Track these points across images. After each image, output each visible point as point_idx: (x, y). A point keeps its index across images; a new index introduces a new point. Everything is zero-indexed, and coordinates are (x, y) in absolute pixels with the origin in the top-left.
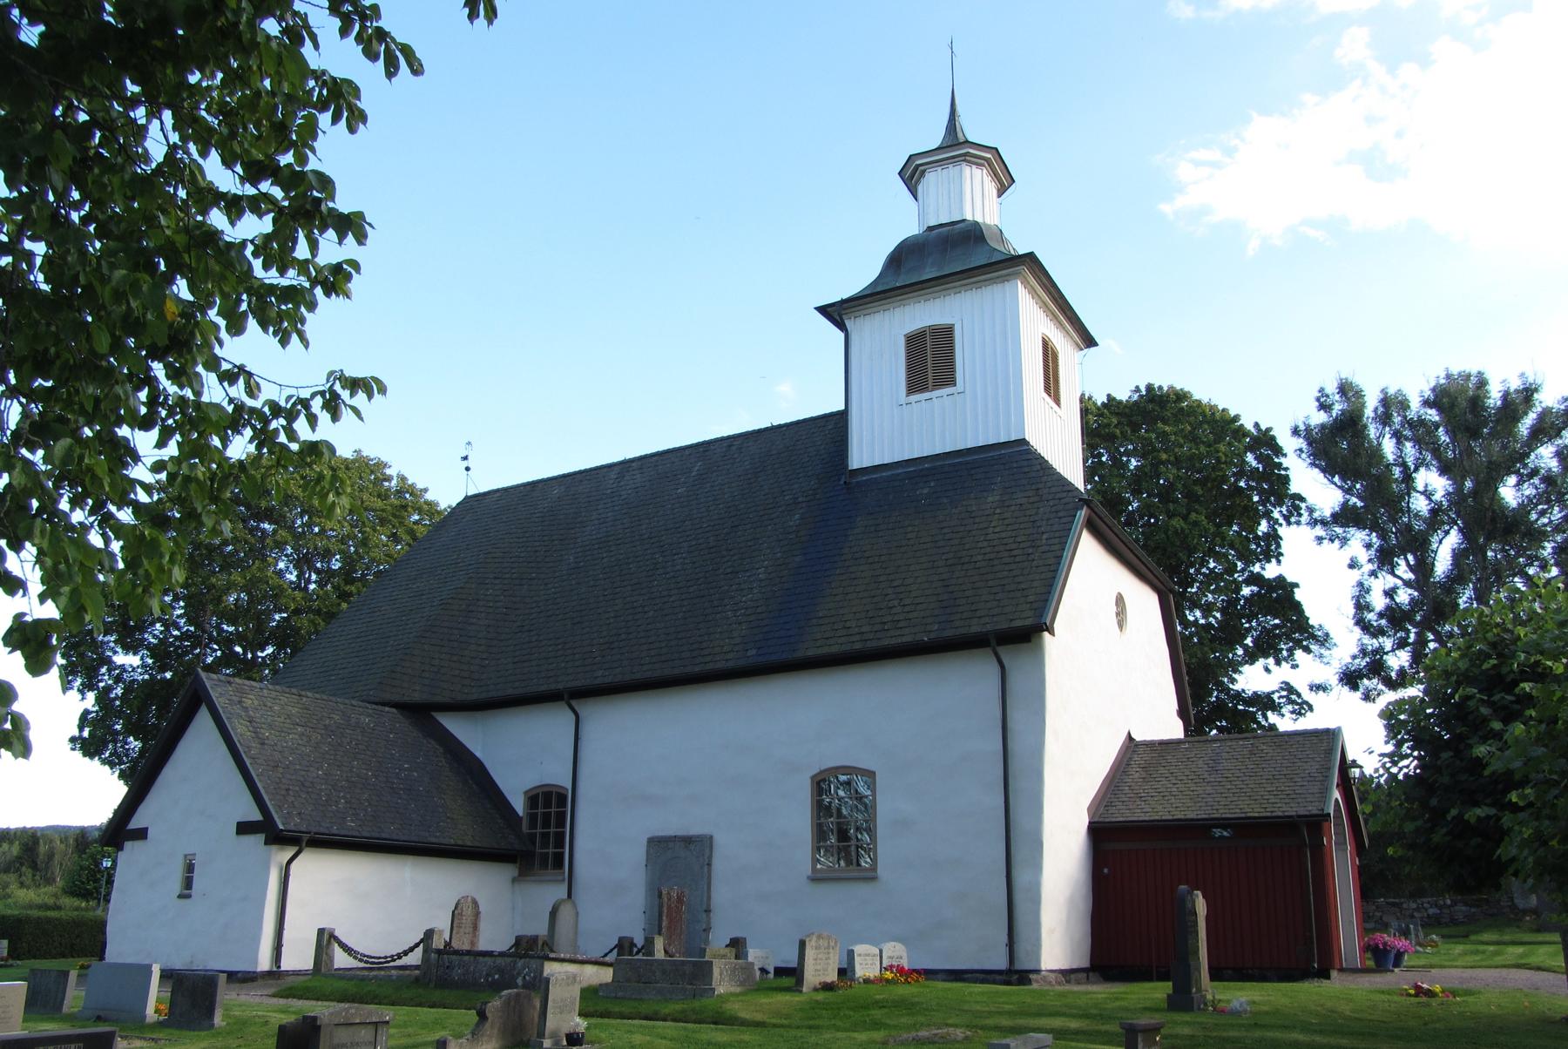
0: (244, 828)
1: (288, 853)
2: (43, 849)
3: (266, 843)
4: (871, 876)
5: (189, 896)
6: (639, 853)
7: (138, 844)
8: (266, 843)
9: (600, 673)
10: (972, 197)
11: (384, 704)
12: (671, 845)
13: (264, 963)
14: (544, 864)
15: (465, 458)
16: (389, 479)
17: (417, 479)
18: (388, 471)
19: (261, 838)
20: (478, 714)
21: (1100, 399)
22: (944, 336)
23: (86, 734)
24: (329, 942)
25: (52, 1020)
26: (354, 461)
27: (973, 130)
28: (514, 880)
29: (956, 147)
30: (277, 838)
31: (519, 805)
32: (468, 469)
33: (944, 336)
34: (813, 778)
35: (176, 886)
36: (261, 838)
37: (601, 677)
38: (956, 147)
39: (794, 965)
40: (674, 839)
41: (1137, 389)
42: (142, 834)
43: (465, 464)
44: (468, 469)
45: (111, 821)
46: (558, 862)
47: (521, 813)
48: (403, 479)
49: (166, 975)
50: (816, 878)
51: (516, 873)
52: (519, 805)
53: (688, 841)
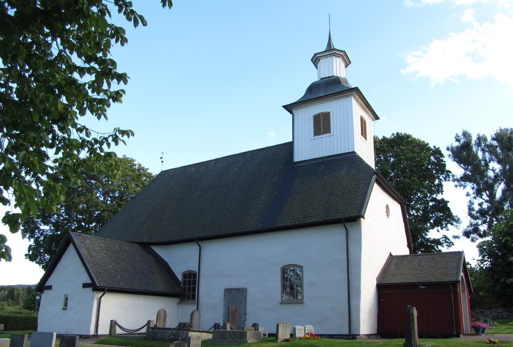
0: (85, 286)
1: (100, 294)
2: (16, 293)
5: (66, 309)
6: (221, 294)
9: (208, 232)
11: (133, 243)
15: (161, 158)
16: (135, 165)
17: (145, 165)
18: (135, 163)
19: (91, 289)
20: (166, 246)
23: (31, 253)
24: (114, 325)
26: (123, 159)
27: (336, 45)
29: (331, 51)
30: (96, 289)
31: (180, 278)
32: (162, 162)
34: (281, 268)
36: (91, 289)
37: (208, 233)
38: (331, 51)
42: (50, 288)
43: (161, 160)
44: (162, 162)
45: (39, 283)
46: (193, 297)
48: (140, 165)
49: (58, 336)
53: (238, 290)
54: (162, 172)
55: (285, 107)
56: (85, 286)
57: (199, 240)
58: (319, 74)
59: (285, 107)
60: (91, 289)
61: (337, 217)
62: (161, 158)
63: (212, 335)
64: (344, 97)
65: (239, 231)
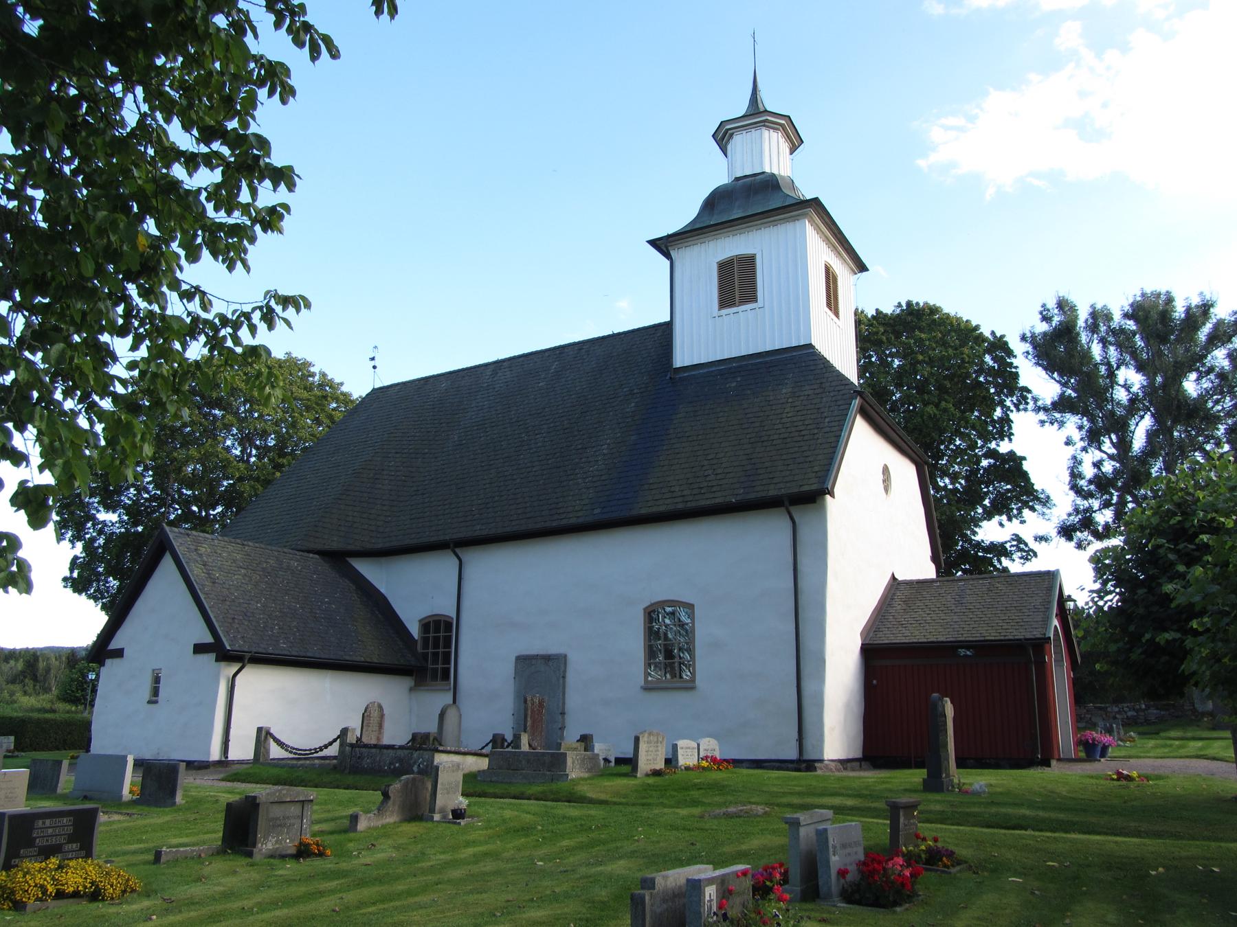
0: (199, 649)
1: (234, 668)
2: (42, 665)
4: (690, 686)
5: (156, 702)
6: (509, 668)
7: (116, 661)
10: (770, 155)
11: (309, 552)
14: (434, 678)
15: (373, 359)
16: (313, 375)
17: (335, 375)
18: (312, 369)
20: (383, 559)
21: (870, 312)
23: (75, 575)
27: (770, 102)
28: (411, 690)
29: (757, 115)
30: (225, 656)
31: (415, 630)
32: (374, 367)
34: (645, 609)
35: (146, 694)
36: (213, 656)
37: (479, 530)
38: (757, 115)
41: (900, 305)
43: (373, 363)
44: (374, 367)
46: (445, 675)
47: (416, 636)
48: (324, 375)
49: (138, 763)
50: (648, 688)
51: (413, 684)
52: (415, 630)
53: (547, 658)
54: (374, 390)
56: (199, 649)
57: (457, 544)
60: (212, 656)
62: (373, 359)
63: (487, 760)
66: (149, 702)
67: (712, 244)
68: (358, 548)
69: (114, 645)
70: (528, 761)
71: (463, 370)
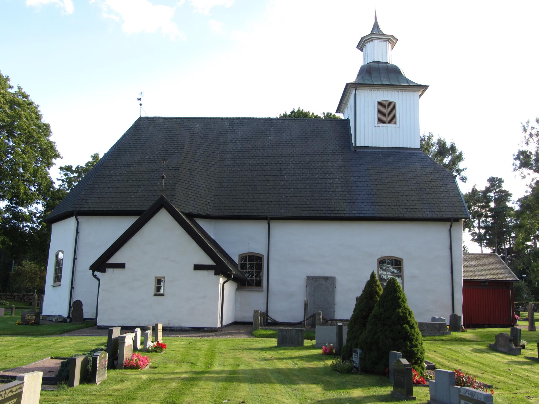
3: (216, 274)
6: (302, 282)
8: (216, 274)
9: (283, 211)
10: (379, 53)
12: (318, 280)
13: (219, 325)
15: (140, 99)
20: (213, 221)
21: (315, 114)
22: (392, 106)
25: (301, 349)
27: (385, 29)
29: (376, 33)
31: (237, 260)
32: (141, 105)
33: (392, 106)
34: (378, 259)
35: (153, 290)
37: (283, 213)
38: (376, 33)
39: (94, 317)
40: (320, 277)
41: (324, 114)
43: (139, 102)
44: (141, 105)
46: (259, 284)
47: (238, 263)
48: (19, 88)
53: (326, 279)
54: (140, 118)
55: (428, 86)
57: (269, 218)
58: (365, 57)
59: (428, 86)
61: (264, 214)
62: (140, 99)
63: (220, 326)
64: (410, 91)
65: (328, 215)
66: (155, 295)
67: (366, 92)
68: (204, 214)
69: (113, 260)
70: (428, 327)
71: (211, 119)
